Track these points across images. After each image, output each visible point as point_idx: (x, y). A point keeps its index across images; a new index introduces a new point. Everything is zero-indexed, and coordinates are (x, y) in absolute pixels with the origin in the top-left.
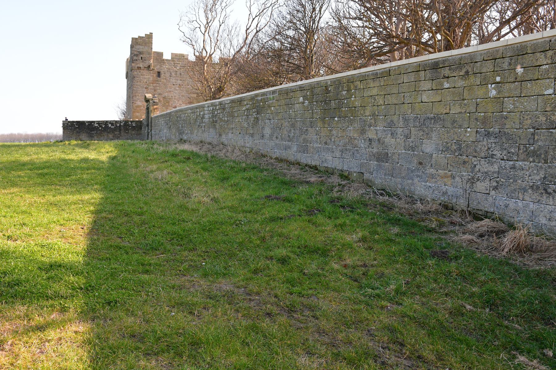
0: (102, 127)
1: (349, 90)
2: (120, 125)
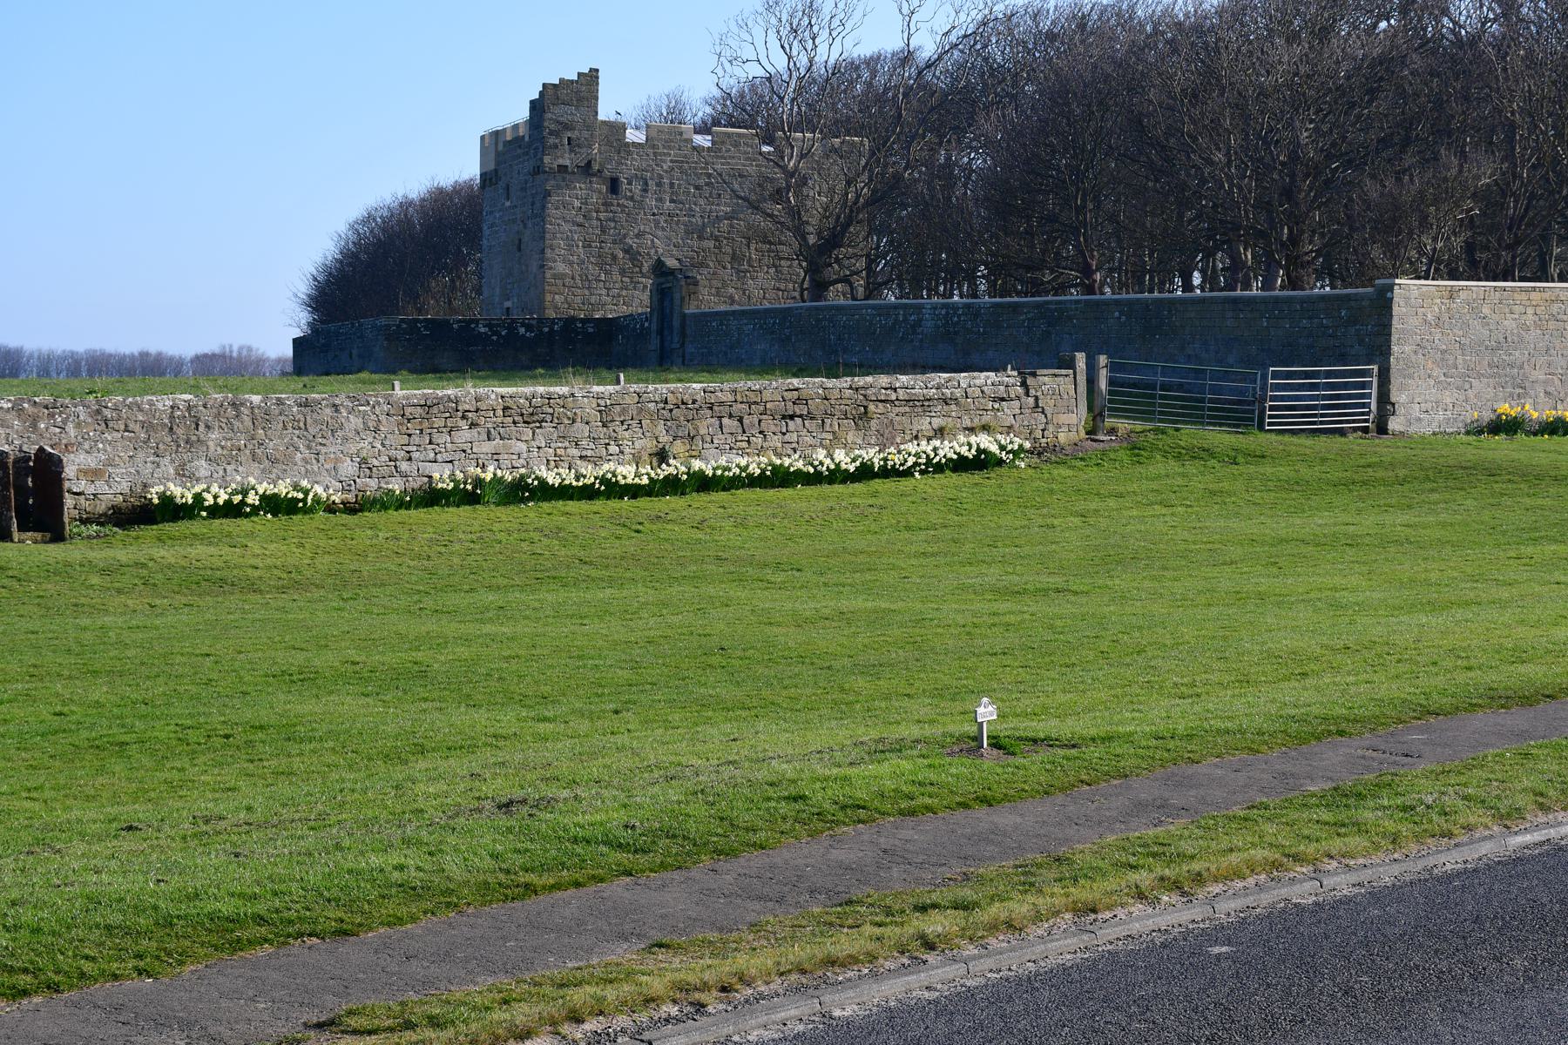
0: (499, 335)
1: (1170, 311)
2: (552, 329)
